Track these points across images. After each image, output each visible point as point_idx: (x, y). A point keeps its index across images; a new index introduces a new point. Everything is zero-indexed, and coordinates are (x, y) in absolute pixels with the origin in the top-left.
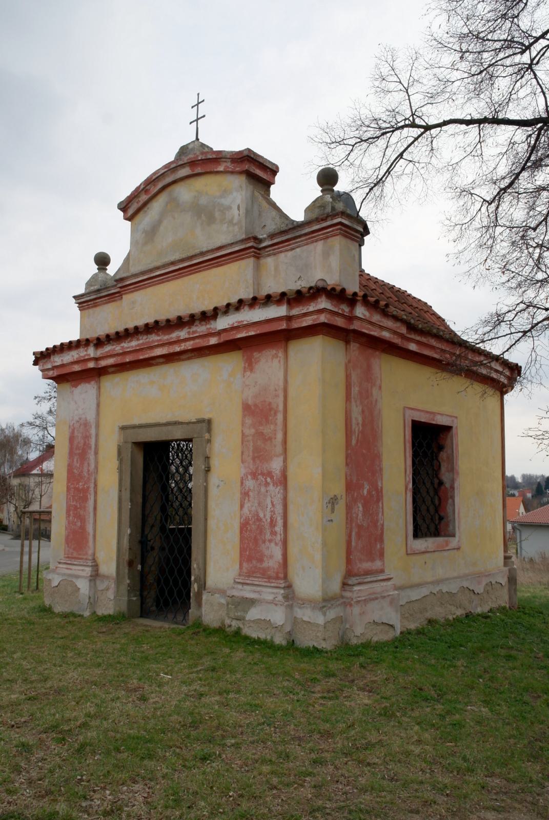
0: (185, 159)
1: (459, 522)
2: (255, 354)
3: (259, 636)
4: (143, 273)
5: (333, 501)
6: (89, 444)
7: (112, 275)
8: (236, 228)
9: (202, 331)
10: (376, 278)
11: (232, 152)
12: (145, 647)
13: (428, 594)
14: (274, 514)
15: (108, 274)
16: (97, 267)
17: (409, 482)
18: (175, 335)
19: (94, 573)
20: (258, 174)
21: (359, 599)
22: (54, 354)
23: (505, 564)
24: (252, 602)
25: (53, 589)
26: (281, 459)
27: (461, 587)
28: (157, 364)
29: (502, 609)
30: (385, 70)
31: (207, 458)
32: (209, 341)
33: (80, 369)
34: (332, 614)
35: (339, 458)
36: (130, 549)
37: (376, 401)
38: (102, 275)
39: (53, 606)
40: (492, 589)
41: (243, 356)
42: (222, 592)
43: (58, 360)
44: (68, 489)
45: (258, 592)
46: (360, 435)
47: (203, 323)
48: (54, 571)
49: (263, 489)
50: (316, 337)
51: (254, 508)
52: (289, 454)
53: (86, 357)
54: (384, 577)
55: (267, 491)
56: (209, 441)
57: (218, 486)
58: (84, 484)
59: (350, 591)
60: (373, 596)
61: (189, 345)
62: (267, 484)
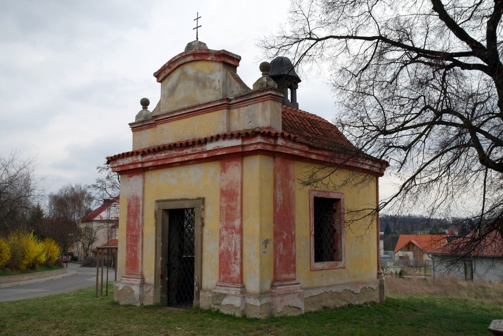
0: (190, 52)
1: (345, 253)
2: (226, 163)
3: (228, 313)
4: (168, 114)
5: (266, 242)
6: (138, 210)
7: (151, 112)
8: (218, 93)
9: (199, 150)
10: (305, 112)
11: (215, 51)
12: (169, 318)
13: (323, 292)
14: (236, 249)
15: (148, 111)
16: (142, 107)
17: (312, 231)
18: (185, 151)
19: (142, 282)
20: (229, 62)
21: (279, 293)
22: (119, 159)
23: (378, 277)
24: (225, 295)
25: (119, 292)
26: (239, 220)
27: (344, 290)
28: (176, 166)
29: (373, 303)
30: (297, 8)
31: (202, 219)
32: (203, 155)
33: (133, 168)
34: (264, 301)
35: (269, 219)
36: (162, 268)
37: (292, 187)
38: (145, 112)
39: (119, 301)
40: (366, 291)
41: (221, 164)
42: (210, 291)
43: (121, 162)
44: (127, 236)
45: (228, 290)
46: (282, 206)
47: (200, 146)
48: (119, 282)
49: (231, 236)
50: (257, 156)
51: (226, 246)
52: (244, 217)
53: (137, 162)
54: (295, 282)
55: (233, 237)
56: (203, 209)
57: (208, 234)
58: (136, 233)
59: (275, 289)
60: (288, 292)
61: (192, 157)
62: (232, 233)
